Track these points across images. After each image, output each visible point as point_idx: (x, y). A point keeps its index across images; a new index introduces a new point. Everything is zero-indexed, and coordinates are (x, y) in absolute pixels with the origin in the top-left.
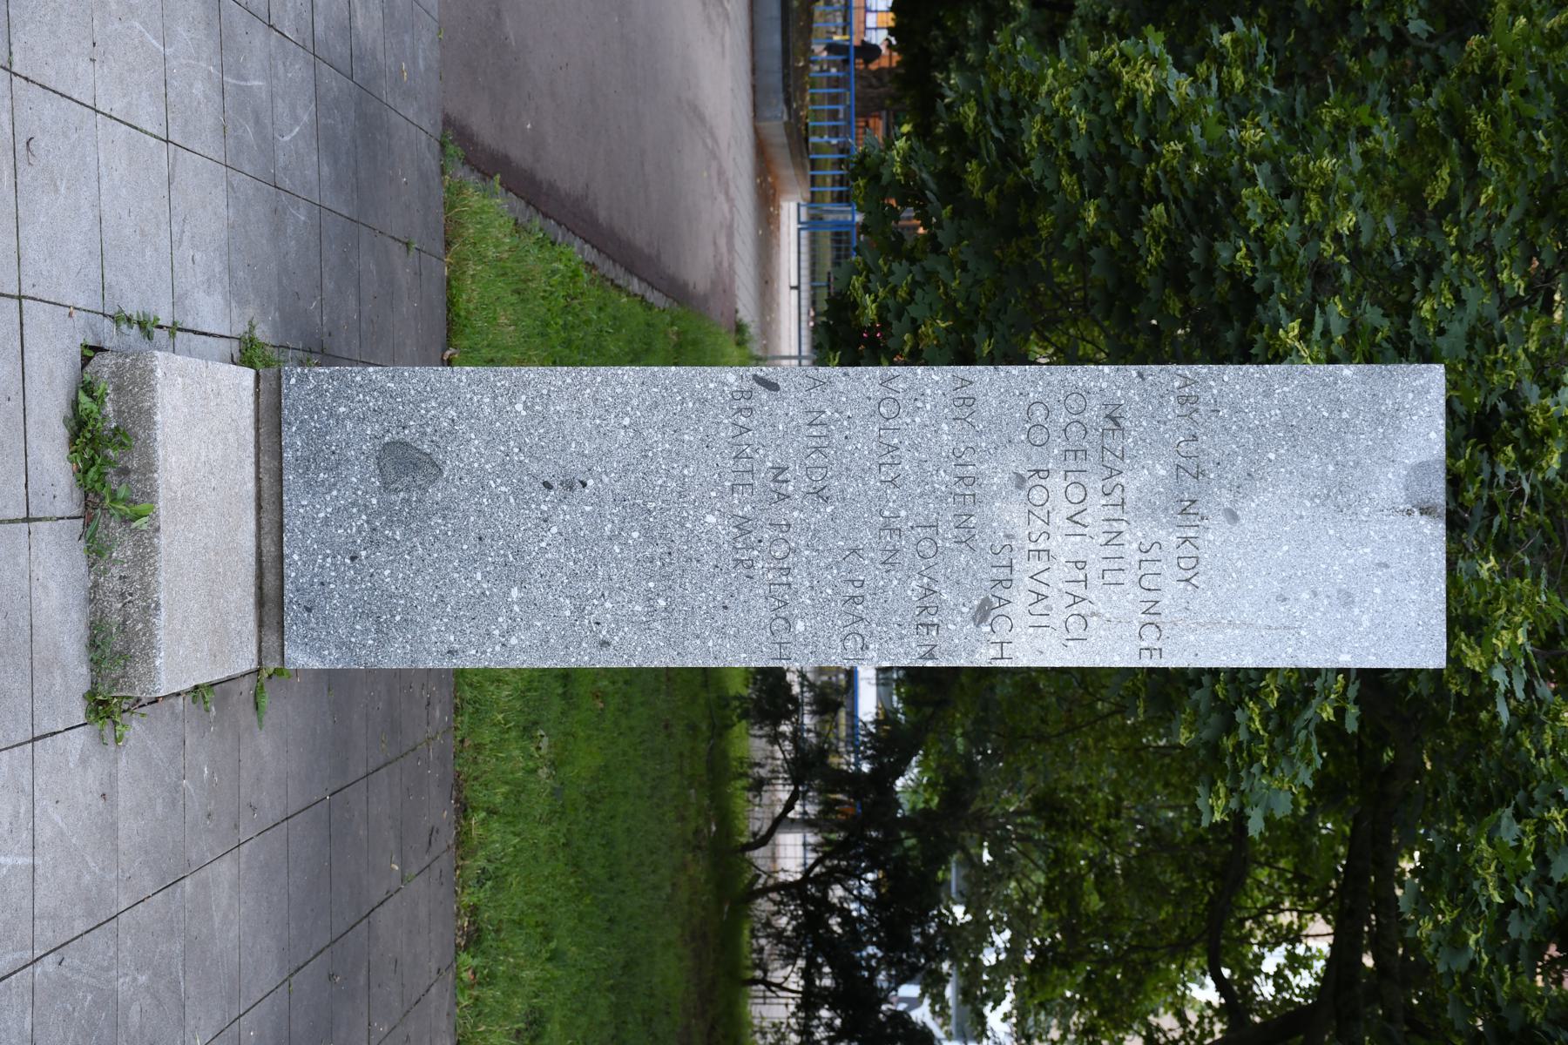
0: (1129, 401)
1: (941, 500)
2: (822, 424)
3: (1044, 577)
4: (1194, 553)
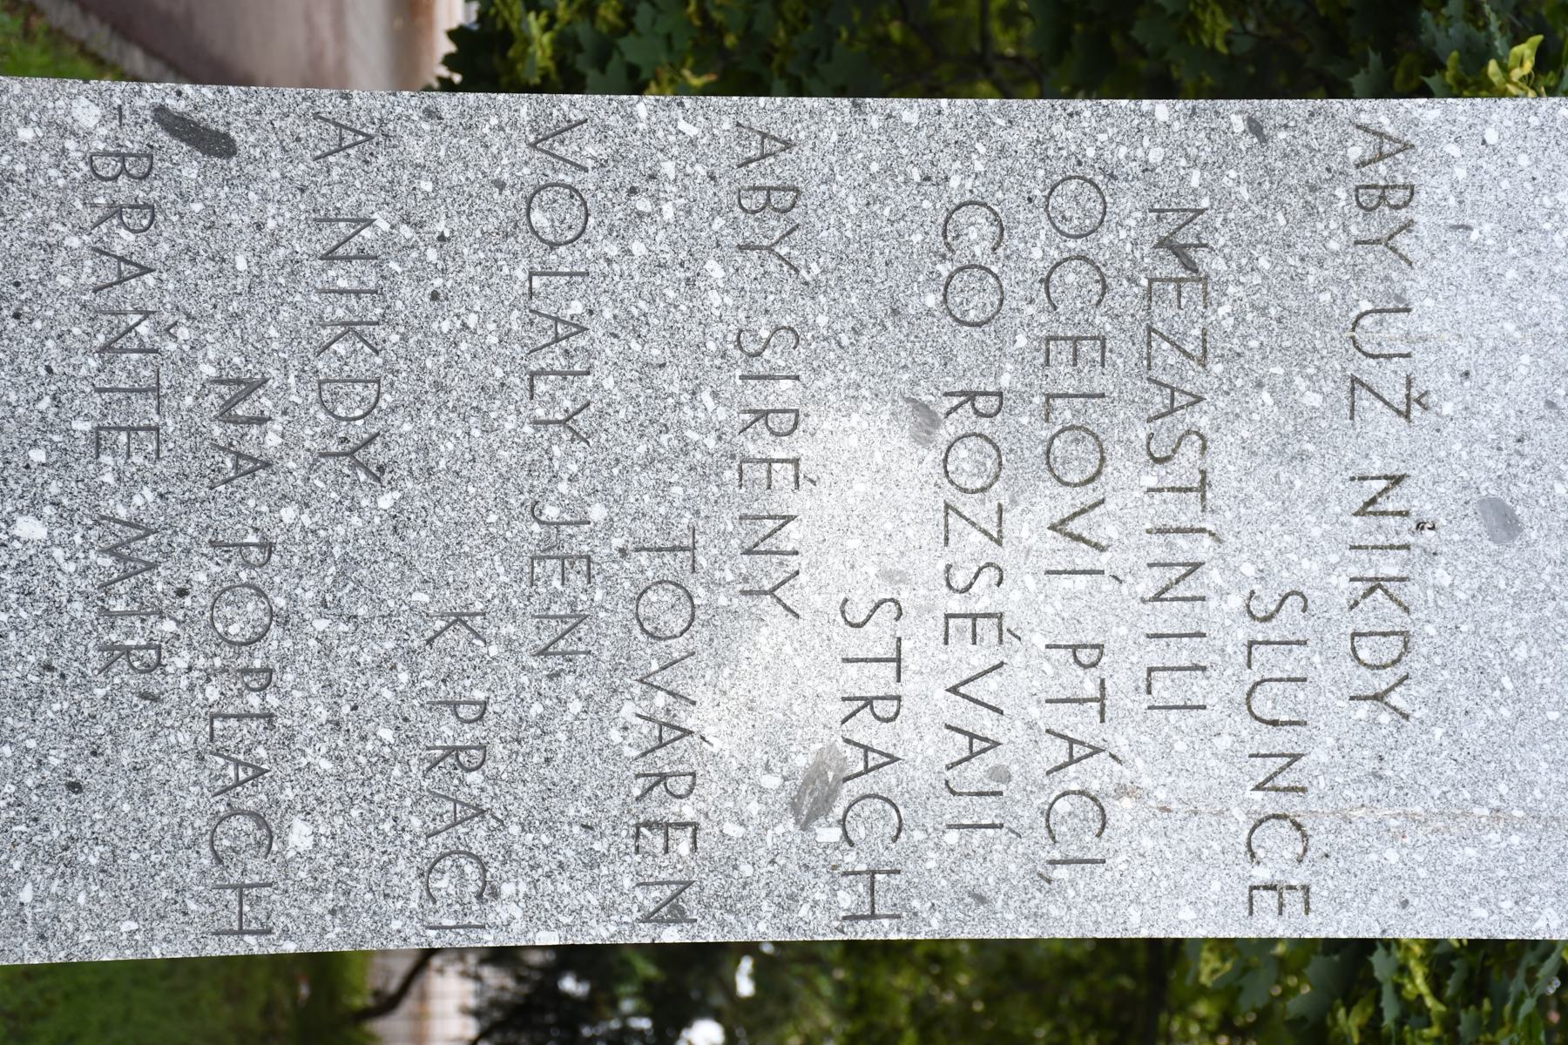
0: (1224, 199)
1: (702, 473)
2: (362, 256)
3: (985, 689)
4: (1398, 620)
